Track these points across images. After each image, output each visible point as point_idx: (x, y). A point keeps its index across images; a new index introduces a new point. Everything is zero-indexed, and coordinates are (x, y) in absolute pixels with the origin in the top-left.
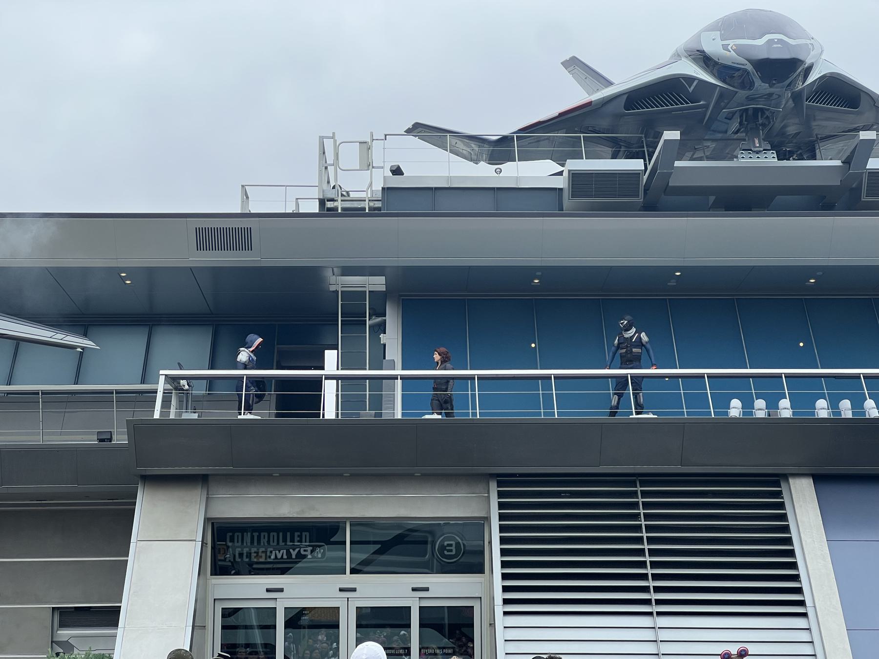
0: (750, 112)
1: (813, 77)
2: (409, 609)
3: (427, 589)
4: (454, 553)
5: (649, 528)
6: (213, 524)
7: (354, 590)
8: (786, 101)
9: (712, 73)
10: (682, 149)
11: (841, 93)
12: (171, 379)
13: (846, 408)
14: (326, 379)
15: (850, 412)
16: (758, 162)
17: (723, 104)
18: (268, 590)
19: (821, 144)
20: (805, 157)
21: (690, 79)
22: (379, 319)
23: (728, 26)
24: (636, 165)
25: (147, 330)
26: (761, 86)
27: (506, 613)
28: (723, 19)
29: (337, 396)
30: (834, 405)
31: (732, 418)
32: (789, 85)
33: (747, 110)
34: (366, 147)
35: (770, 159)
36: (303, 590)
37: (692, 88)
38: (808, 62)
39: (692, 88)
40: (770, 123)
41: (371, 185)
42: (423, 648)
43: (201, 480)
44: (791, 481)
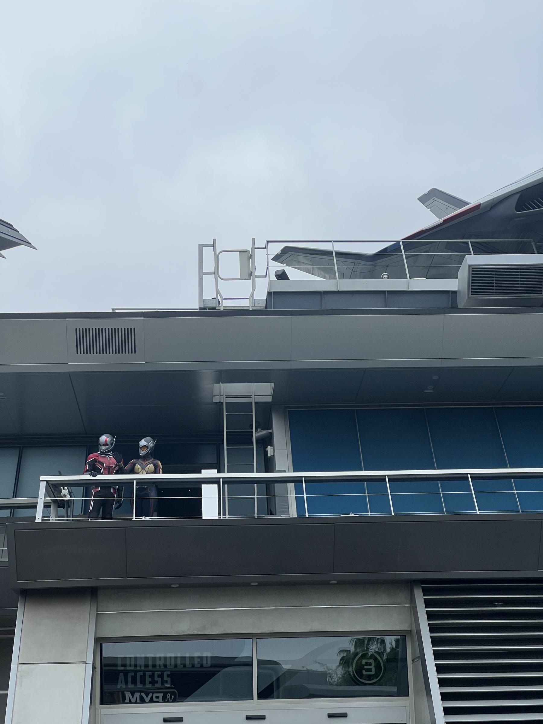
4: (373, 672)
22: (264, 432)
25: (16, 453)
34: (247, 256)
41: (252, 295)
43: (88, 594)
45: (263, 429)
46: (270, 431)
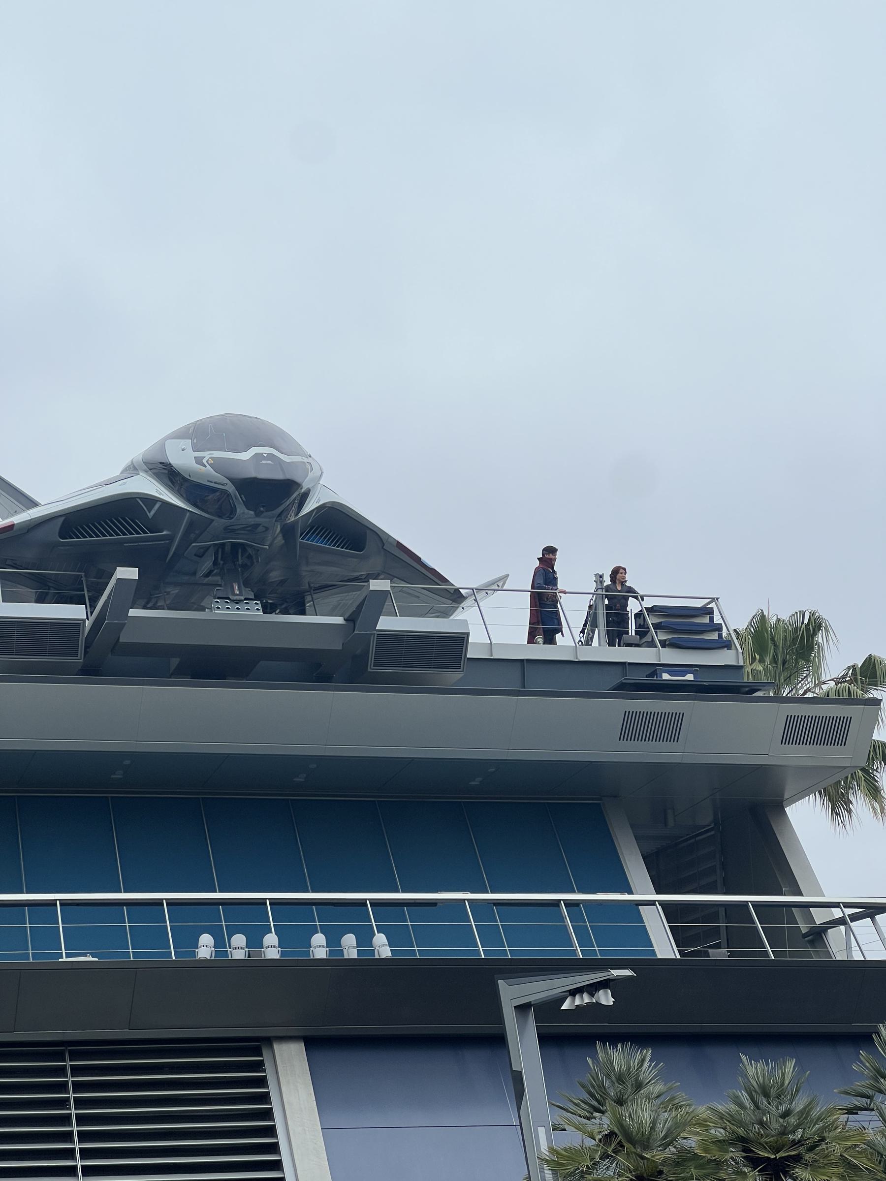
0: (228, 548)
1: (310, 506)
5: (79, 1103)
8: (275, 537)
9: (179, 493)
10: (144, 593)
11: (344, 530)
13: (350, 946)
15: (356, 950)
16: (235, 615)
17: (192, 536)
19: (315, 596)
20: (291, 612)
21: (150, 501)
23: (201, 434)
24: (75, 612)
26: (244, 514)
28: (195, 424)
30: (333, 941)
31: (200, 961)
32: (280, 515)
33: (223, 545)
35: (253, 612)
37: (153, 512)
38: (305, 486)
39: (153, 512)
40: (252, 563)
41: (565, 592)
44: (276, 1046)
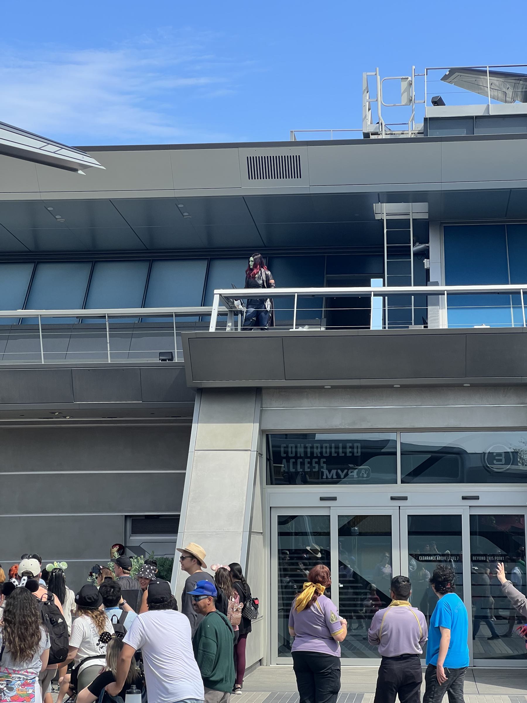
2: (458, 518)
3: (477, 498)
6: (267, 436)
7: (405, 498)
12: (226, 300)
14: (375, 295)
18: (322, 499)
22: (423, 246)
27: (275, 479)
29: (384, 311)
36: (357, 498)
42: (475, 555)
45: (421, 243)
46: (427, 245)
